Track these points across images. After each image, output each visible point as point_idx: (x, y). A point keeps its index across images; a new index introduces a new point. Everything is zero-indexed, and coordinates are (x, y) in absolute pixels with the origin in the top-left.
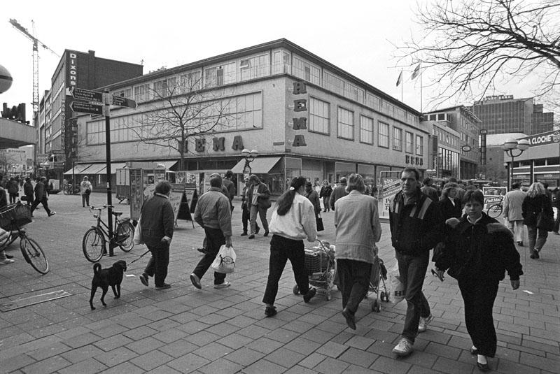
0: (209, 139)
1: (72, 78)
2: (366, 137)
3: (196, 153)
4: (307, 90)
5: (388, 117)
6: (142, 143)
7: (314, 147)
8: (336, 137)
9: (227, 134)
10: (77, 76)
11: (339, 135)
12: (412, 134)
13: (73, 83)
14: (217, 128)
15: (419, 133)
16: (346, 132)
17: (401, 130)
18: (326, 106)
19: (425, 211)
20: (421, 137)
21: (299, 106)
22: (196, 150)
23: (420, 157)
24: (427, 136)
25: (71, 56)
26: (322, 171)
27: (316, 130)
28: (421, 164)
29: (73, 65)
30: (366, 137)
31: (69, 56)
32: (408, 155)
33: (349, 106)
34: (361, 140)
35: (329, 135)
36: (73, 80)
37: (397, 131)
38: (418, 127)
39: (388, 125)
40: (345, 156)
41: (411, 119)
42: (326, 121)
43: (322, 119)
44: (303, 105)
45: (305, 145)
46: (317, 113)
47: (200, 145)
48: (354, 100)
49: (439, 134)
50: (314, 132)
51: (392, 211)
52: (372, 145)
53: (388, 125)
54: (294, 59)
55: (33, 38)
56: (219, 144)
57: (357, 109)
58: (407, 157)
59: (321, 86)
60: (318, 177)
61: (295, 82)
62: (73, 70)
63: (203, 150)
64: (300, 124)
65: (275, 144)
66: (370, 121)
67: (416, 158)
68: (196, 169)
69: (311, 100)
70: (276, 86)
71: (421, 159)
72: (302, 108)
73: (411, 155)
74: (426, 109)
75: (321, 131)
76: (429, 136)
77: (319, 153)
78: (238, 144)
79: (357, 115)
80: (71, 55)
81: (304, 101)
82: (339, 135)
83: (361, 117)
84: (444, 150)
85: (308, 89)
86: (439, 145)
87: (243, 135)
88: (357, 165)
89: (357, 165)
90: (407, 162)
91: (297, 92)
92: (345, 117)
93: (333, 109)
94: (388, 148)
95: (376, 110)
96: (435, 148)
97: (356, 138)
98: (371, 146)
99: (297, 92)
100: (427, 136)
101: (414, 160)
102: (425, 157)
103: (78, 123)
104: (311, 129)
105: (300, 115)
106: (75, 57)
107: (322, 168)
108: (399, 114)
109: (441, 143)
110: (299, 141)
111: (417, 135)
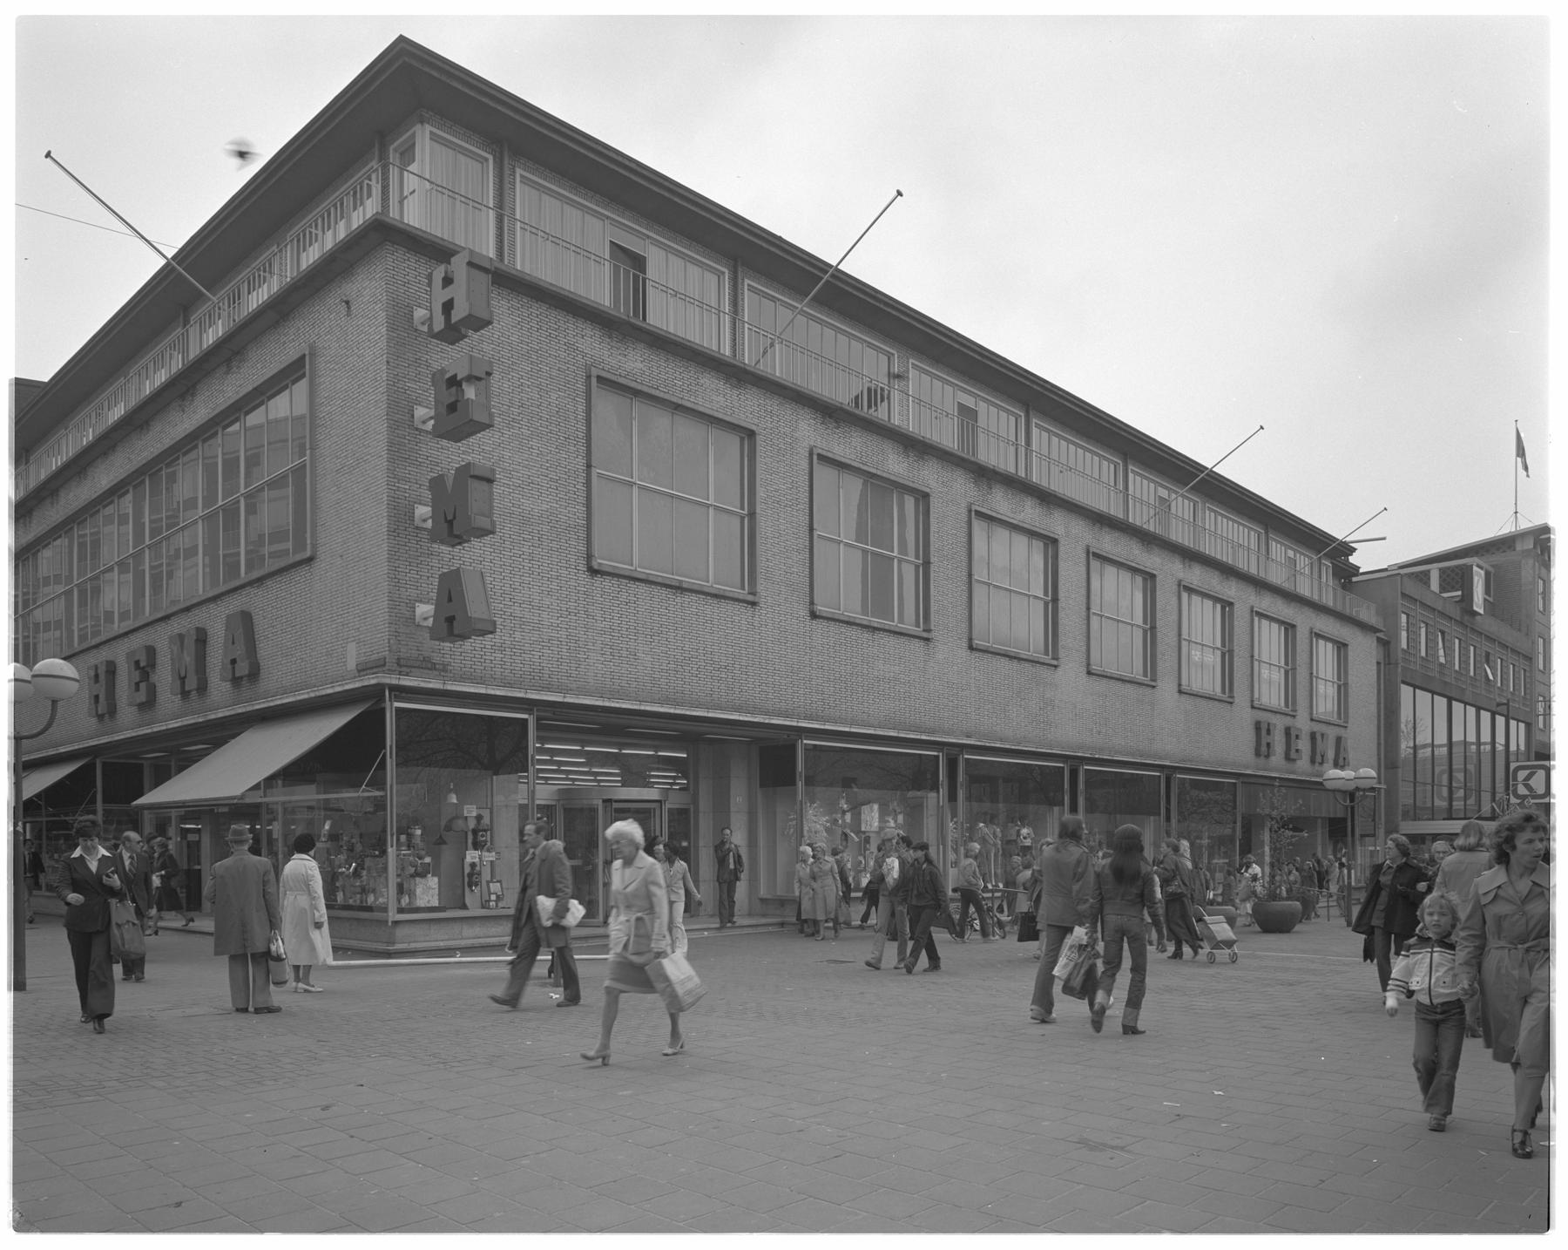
5: (1228, 571)
12: (1290, 628)
20: (1341, 646)
23: (1332, 733)
38: (1328, 600)
45: (488, 629)
59: (1316, 597)
95: (1241, 565)
101: (1304, 745)
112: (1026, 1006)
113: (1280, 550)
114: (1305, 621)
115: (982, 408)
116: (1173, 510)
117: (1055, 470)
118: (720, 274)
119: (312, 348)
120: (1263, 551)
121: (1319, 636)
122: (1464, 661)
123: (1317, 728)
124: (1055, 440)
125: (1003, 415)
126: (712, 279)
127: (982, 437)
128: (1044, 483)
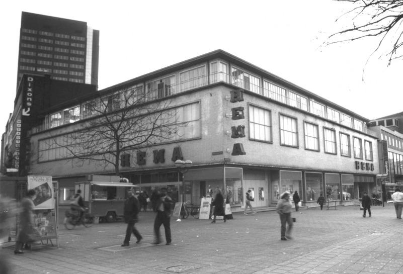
0: (150, 152)
1: (28, 99)
2: (312, 144)
3: (138, 166)
4: (244, 98)
5: (334, 123)
6: (76, 160)
7: (254, 155)
8: (279, 145)
9: (166, 146)
10: (33, 97)
11: (282, 142)
12: (360, 140)
13: (29, 104)
14: (153, 140)
15: (367, 138)
16: (289, 139)
17: (348, 136)
18: (267, 114)
19: (382, 215)
20: (370, 143)
21: (237, 114)
22: (138, 163)
23: (370, 163)
24: (376, 140)
25: (29, 80)
26: (267, 179)
27: (257, 138)
28: (372, 169)
29: (30, 88)
30: (312, 144)
31: (27, 79)
32: (357, 160)
33: (292, 114)
34: (307, 147)
35: (271, 143)
36: (29, 101)
37: (344, 137)
38: (366, 133)
39: (296, 119)
40: (290, 163)
41: (358, 125)
42: (267, 129)
43: (291, 133)
44: (240, 113)
45: (245, 154)
46: (258, 122)
47: (142, 157)
48: (284, 102)
49: (388, 139)
50: (254, 140)
51: (367, 211)
52: (271, 143)
53: (317, 126)
54: (264, 82)
55: (200, 114)
56: (159, 156)
57: (301, 117)
58: (357, 163)
59: (261, 94)
60: (262, 187)
61: (231, 90)
62: (30, 92)
63: (145, 163)
64: (238, 132)
65: (214, 154)
66: (293, 121)
67: (367, 164)
68: (139, 183)
69: (251, 109)
70: (213, 95)
71: (372, 165)
72: (240, 115)
73: (360, 161)
74: (372, 117)
75: (262, 139)
76: (378, 141)
77: (333, 168)
78: (177, 154)
79: (300, 122)
80: (29, 79)
81: (241, 109)
82: (282, 142)
83: (305, 124)
84: (395, 155)
85: (245, 97)
86: (389, 149)
87: (183, 146)
88: (340, 175)
89: (340, 175)
90: (357, 168)
91: (235, 99)
92: (287, 124)
93: (275, 117)
94: (336, 154)
95: (321, 116)
96: (386, 154)
97: (301, 144)
98: (335, 156)
99: (235, 99)
100: (376, 140)
101: (365, 166)
102: (376, 161)
103: (31, 141)
104: (252, 137)
105: (238, 123)
106: (32, 80)
107: (267, 177)
108: (347, 121)
109: (391, 148)
110: (238, 150)
111: (365, 141)
112: (278, 234)
113: (329, 110)
114: (363, 137)
115: (250, 77)
116: (251, 81)
117: (270, 93)
118: (226, 65)
119: (200, 100)
120: (261, 86)
121: (355, 137)
122: (392, 141)
123: (368, 162)
124: (269, 84)
125: (256, 79)
126: (225, 66)
127: (251, 85)
128: (267, 96)
